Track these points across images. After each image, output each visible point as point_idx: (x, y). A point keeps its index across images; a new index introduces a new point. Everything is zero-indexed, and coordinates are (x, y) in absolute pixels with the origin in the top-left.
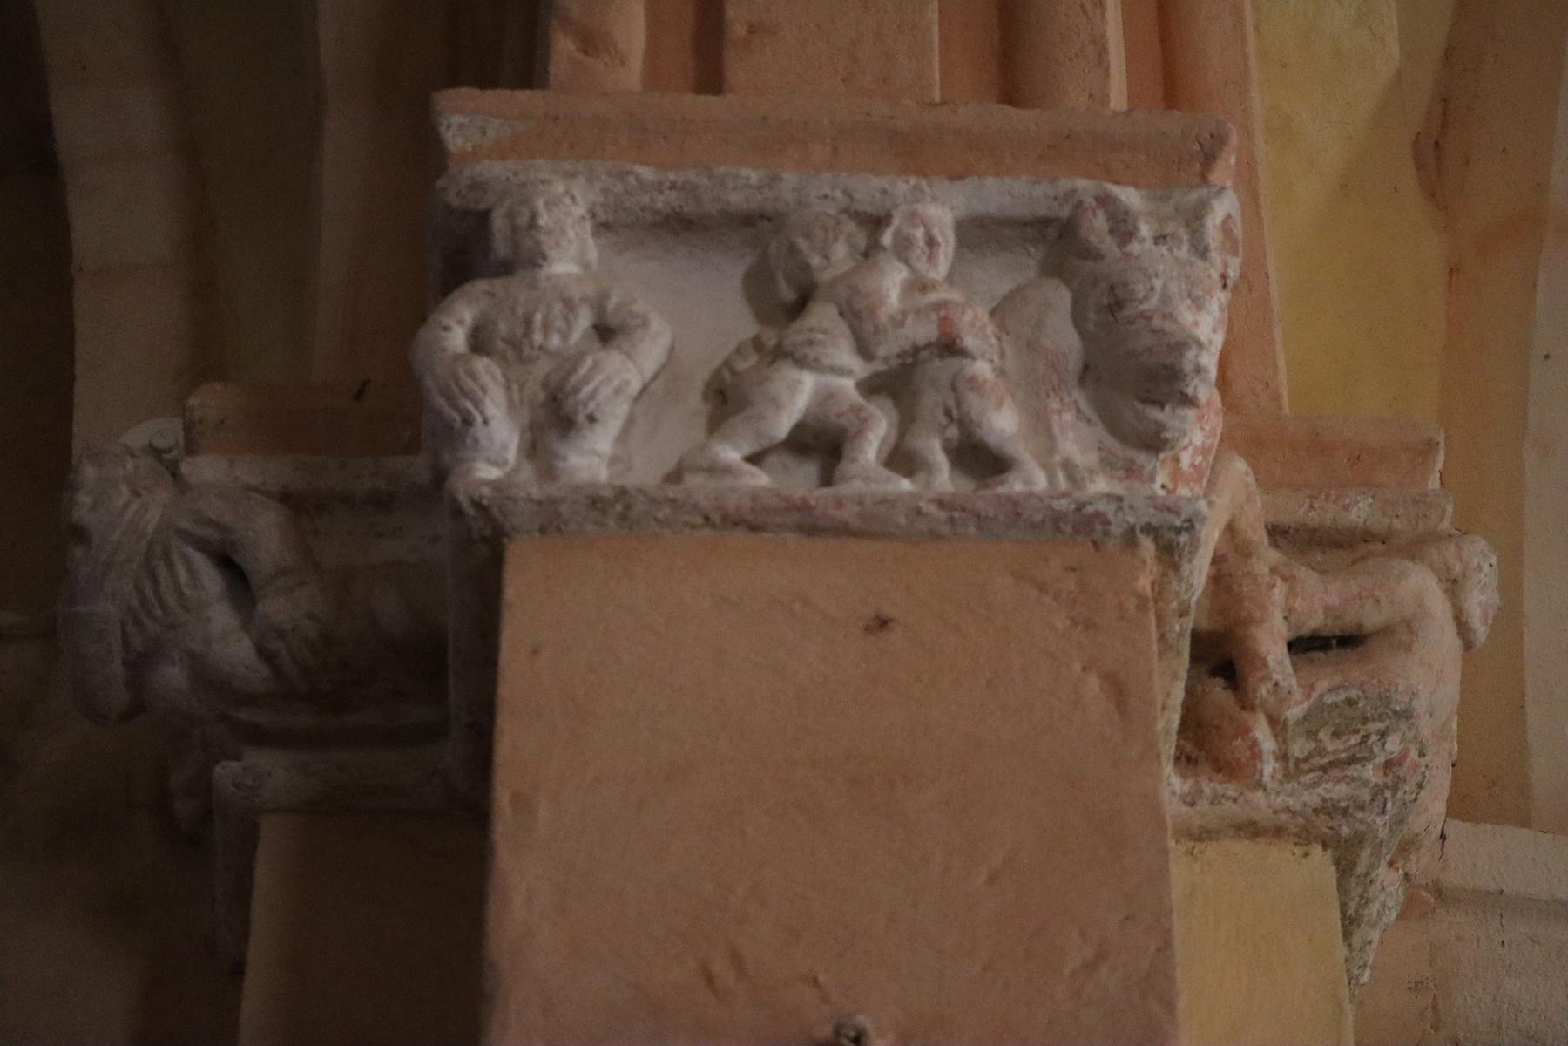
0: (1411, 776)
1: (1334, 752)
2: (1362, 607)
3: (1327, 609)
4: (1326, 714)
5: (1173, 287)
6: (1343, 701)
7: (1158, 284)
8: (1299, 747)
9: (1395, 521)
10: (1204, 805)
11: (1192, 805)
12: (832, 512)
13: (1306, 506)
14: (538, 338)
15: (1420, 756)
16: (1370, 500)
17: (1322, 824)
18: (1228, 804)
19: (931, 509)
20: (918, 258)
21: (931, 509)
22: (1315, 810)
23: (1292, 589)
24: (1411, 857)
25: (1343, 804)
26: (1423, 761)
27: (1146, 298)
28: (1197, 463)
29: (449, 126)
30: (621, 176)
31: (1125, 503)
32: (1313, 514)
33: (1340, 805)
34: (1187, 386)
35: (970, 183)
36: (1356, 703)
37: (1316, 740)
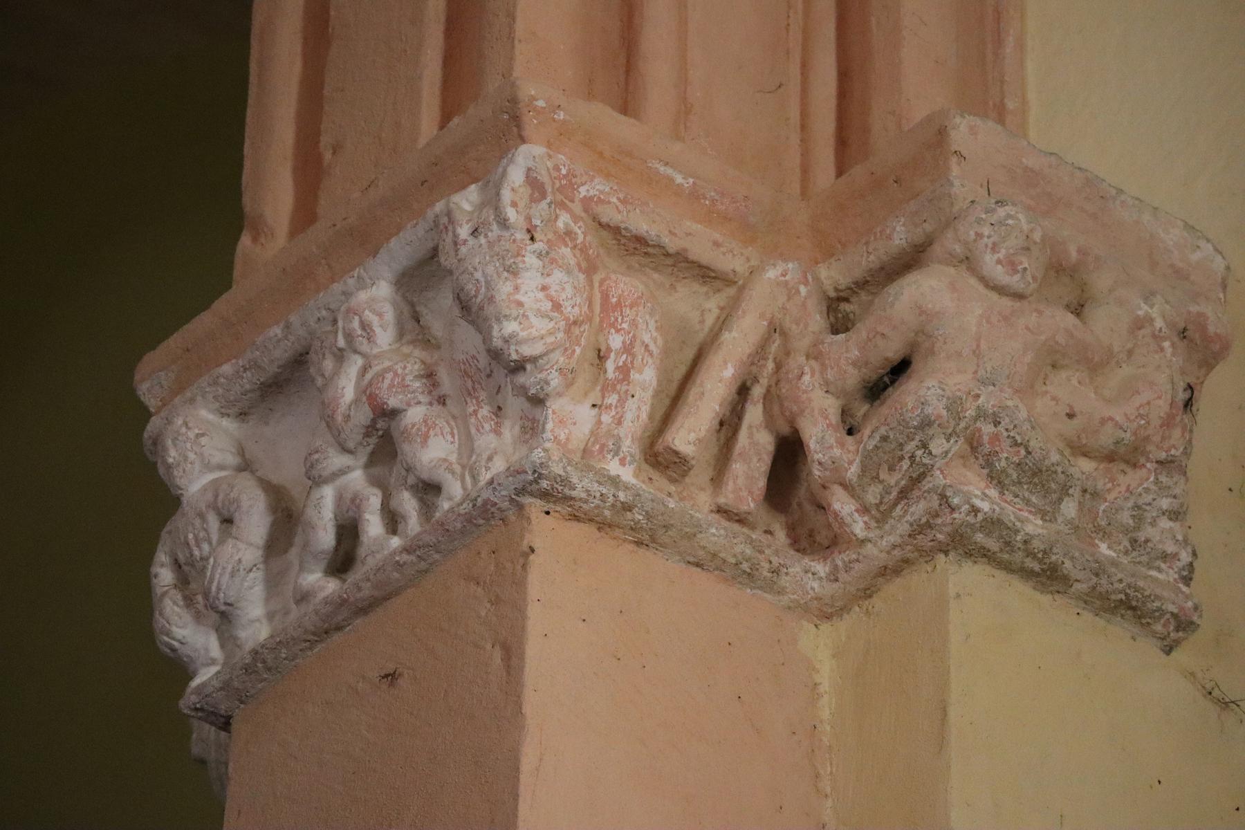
0: (1000, 446)
1: (897, 483)
2: (875, 346)
3: (854, 364)
4: (875, 458)
5: (490, 270)
6: (880, 441)
7: (478, 275)
8: (872, 495)
9: (926, 225)
10: (843, 576)
11: (836, 580)
12: (359, 595)
13: (865, 254)
14: (196, 553)
15: (995, 426)
16: (903, 220)
17: (924, 541)
18: (857, 566)
19: (405, 557)
20: (362, 344)
21: (405, 557)
22: (910, 536)
23: (823, 365)
24: (1148, 449)
25: (924, 520)
26: (1001, 428)
27: (477, 291)
28: (621, 364)
30: (215, 383)
32: (872, 257)
33: (922, 522)
34: (509, 355)
35: (383, 255)
36: (888, 437)
37: (881, 482)
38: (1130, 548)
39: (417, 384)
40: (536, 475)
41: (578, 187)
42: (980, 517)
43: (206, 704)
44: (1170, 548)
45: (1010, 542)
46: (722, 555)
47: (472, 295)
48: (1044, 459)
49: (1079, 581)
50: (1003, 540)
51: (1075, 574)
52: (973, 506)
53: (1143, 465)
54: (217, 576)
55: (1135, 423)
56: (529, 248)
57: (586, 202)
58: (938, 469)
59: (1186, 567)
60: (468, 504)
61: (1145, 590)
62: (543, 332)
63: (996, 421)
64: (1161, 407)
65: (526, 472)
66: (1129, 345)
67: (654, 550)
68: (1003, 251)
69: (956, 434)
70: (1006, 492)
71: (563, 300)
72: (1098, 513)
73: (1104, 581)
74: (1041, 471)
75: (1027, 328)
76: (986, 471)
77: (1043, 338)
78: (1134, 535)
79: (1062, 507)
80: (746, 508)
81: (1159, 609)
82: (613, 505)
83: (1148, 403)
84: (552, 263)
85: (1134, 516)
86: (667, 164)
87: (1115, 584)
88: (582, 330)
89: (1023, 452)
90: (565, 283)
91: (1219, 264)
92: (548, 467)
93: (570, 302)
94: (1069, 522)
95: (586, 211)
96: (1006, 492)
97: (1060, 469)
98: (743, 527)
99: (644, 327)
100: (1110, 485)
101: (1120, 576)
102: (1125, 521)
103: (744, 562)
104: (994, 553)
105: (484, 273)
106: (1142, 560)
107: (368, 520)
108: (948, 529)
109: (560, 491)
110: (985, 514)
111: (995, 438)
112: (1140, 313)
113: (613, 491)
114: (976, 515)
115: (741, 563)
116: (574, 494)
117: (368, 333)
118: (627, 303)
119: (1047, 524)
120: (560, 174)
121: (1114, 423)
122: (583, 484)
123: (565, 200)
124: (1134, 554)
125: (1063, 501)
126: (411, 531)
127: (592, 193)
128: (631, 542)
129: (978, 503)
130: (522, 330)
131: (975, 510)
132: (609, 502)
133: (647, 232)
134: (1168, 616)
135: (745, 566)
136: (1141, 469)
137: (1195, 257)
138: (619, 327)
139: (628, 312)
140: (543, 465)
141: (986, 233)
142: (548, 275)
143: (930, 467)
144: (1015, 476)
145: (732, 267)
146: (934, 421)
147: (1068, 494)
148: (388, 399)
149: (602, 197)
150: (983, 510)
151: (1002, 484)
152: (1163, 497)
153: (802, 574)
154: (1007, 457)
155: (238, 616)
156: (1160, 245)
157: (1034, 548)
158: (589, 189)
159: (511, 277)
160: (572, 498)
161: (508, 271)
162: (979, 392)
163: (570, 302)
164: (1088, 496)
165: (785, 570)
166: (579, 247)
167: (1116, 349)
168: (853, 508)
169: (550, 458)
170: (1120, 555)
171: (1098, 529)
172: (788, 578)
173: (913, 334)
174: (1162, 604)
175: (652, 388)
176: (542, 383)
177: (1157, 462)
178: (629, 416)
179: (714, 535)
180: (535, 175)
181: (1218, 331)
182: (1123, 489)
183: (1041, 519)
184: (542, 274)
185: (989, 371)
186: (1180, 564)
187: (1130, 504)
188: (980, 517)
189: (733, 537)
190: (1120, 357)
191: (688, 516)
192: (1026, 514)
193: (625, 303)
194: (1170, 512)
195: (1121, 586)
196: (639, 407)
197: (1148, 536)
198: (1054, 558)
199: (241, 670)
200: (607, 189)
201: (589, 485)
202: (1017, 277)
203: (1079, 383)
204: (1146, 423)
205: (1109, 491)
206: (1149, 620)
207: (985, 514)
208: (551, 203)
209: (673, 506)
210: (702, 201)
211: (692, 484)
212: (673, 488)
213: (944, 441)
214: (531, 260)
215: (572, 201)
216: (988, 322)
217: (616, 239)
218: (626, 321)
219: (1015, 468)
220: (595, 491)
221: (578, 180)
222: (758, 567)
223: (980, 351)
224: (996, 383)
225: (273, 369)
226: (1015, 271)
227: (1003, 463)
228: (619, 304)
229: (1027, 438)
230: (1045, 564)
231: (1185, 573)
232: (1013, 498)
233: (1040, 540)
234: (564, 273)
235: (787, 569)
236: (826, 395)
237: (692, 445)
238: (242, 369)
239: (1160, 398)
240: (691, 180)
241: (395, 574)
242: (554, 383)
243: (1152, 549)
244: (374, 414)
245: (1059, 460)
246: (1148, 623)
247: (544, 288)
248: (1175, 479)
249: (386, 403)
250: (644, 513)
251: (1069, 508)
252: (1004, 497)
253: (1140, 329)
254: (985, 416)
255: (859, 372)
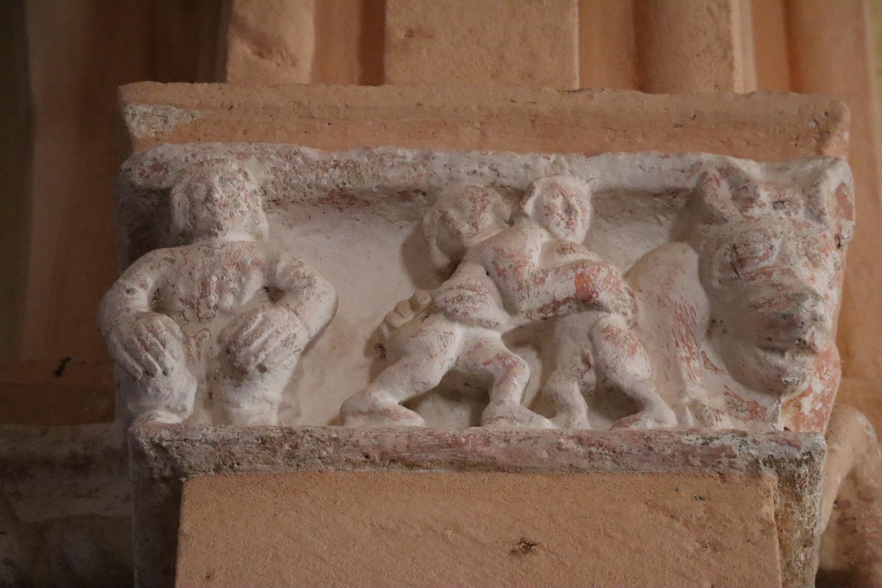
5: (791, 246)
7: (776, 243)
19: (571, 444)
27: (766, 256)
29: (134, 115)
30: (289, 158)
31: (749, 439)
34: (805, 333)
35: (604, 160)
40: (805, 457)
43: (177, 448)
47: (758, 256)
54: (265, 336)
60: (697, 439)
65: (799, 448)
105: (783, 245)
107: (515, 385)
117: (570, 219)
126: (578, 425)
148: (601, 291)
155: (255, 385)
159: (810, 265)
161: (810, 259)
180: (846, 193)
199: (257, 439)
225: (371, 184)
238: (333, 163)
241: (544, 452)
244: (576, 295)
249: (597, 293)
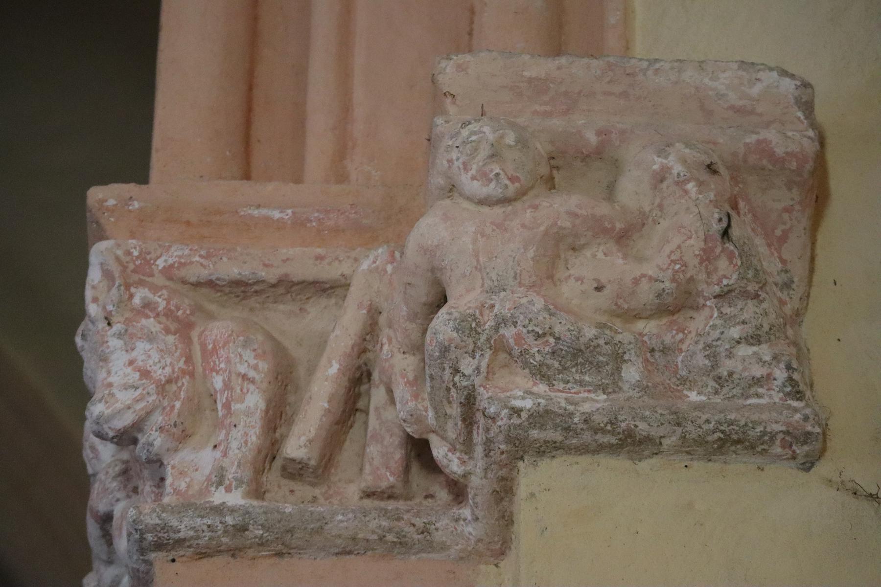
24: (700, 289)
26: (520, 327)
28: (224, 401)
38: (717, 386)
39: (115, 484)
40: (139, 533)
41: (155, 261)
42: (524, 415)
44: (758, 371)
45: (569, 427)
46: (360, 536)
48: (578, 339)
49: (664, 437)
50: (560, 428)
51: (655, 432)
52: (513, 408)
53: (704, 305)
55: (670, 271)
56: (109, 333)
57: (168, 272)
58: (480, 386)
59: (787, 384)
61: (739, 421)
62: (129, 402)
63: (514, 322)
64: (696, 245)
66: (658, 201)
67: (299, 556)
68: (474, 167)
69: (479, 348)
70: (554, 382)
71: (151, 366)
72: (677, 366)
73: (690, 427)
74: (581, 351)
75: (523, 226)
76: (527, 371)
77: (542, 228)
78: (715, 373)
79: (623, 375)
80: (386, 483)
81: (764, 433)
82: (225, 532)
83: (679, 247)
84: (132, 338)
85: (708, 355)
86: (259, 206)
87: (703, 426)
88: (180, 384)
89: (552, 340)
90: (149, 351)
91: (788, 86)
92: (141, 521)
93: (158, 365)
94: (638, 385)
95: (170, 279)
96: (554, 382)
97: (601, 342)
98: (398, 502)
99: (238, 360)
100: (681, 335)
101: (705, 417)
102: (701, 363)
103: (387, 535)
104: (561, 442)
106: (734, 393)
108: (501, 438)
109: (168, 538)
110: (529, 411)
111: (518, 338)
112: (655, 167)
113: (218, 519)
114: (519, 416)
115: (384, 536)
116: (182, 535)
118: (220, 345)
119: (613, 396)
120: (133, 256)
121: (647, 278)
122: (185, 523)
123: (142, 277)
124: (725, 390)
125: (622, 369)
127: (170, 261)
128: (271, 556)
129: (518, 403)
130: (107, 408)
131: (517, 411)
132: (220, 530)
133: (240, 274)
134: (781, 436)
135: (390, 537)
136: (703, 310)
137: (756, 90)
138: (218, 369)
139: (222, 352)
140: (136, 522)
141: (454, 158)
142: (133, 350)
143: (471, 387)
144: (556, 365)
145: (340, 273)
146: (449, 345)
147: (625, 361)
149: (183, 261)
150: (525, 407)
151: (546, 376)
152: (730, 326)
153: (453, 524)
154: (539, 350)
156: (710, 93)
157: (599, 424)
158: (167, 258)
160: (184, 540)
162: (493, 302)
163: (158, 365)
164: (657, 354)
165: (433, 527)
166: (162, 313)
167: (647, 209)
168: (446, 449)
169: (140, 513)
170: (711, 397)
171: (683, 381)
172: (440, 532)
173: (430, 274)
174: (765, 428)
175: (259, 411)
176: (146, 447)
177: (715, 297)
178: (234, 445)
179: (341, 521)
181: (789, 150)
182: (693, 334)
183: (604, 393)
184: (127, 351)
185: (495, 279)
186: (779, 383)
187: (701, 346)
188: (524, 415)
189: (364, 516)
190: (654, 215)
191: (308, 514)
192: (586, 395)
193: (218, 345)
194: (746, 339)
195: (711, 425)
196: (245, 433)
197: (728, 369)
198: (623, 425)
200: (187, 252)
201: (191, 522)
202: (492, 185)
203: (605, 254)
204: (682, 266)
205: (682, 341)
206: (763, 447)
207: (529, 411)
208: (120, 286)
209: (290, 510)
210: (309, 225)
211: (340, 481)
212: (317, 492)
213: (471, 359)
214: (114, 343)
215: (152, 275)
216: (483, 236)
217: (218, 291)
218: (222, 361)
219: (552, 357)
220: (200, 526)
221: (153, 255)
222: (403, 533)
223: (480, 265)
224: (505, 287)
226: (490, 181)
227: (538, 357)
228: (215, 349)
229: (547, 326)
230: (619, 433)
231: (789, 389)
232: (565, 385)
233: (600, 413)
234: (145, 342)
235: (434, 525)
236: (405, 356)
237: (303, 448)
239: (690, 238)
240: (289, 211)
242: (158, 443)
243: (740, 379)
245: (596, 334)
246: (764, 450)
247: (131, 363)
248: (739, 307)
250: (260, 527)
251: (631, 373)
252: (555, 387)
253: (662, 181)
254: (504, 321)
255: (416, 324)
